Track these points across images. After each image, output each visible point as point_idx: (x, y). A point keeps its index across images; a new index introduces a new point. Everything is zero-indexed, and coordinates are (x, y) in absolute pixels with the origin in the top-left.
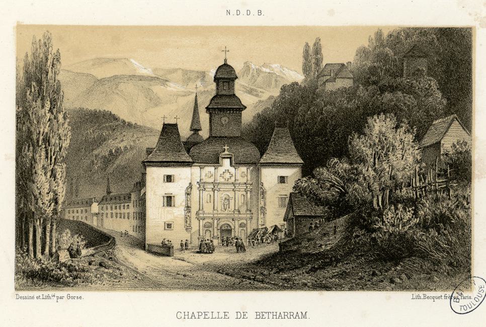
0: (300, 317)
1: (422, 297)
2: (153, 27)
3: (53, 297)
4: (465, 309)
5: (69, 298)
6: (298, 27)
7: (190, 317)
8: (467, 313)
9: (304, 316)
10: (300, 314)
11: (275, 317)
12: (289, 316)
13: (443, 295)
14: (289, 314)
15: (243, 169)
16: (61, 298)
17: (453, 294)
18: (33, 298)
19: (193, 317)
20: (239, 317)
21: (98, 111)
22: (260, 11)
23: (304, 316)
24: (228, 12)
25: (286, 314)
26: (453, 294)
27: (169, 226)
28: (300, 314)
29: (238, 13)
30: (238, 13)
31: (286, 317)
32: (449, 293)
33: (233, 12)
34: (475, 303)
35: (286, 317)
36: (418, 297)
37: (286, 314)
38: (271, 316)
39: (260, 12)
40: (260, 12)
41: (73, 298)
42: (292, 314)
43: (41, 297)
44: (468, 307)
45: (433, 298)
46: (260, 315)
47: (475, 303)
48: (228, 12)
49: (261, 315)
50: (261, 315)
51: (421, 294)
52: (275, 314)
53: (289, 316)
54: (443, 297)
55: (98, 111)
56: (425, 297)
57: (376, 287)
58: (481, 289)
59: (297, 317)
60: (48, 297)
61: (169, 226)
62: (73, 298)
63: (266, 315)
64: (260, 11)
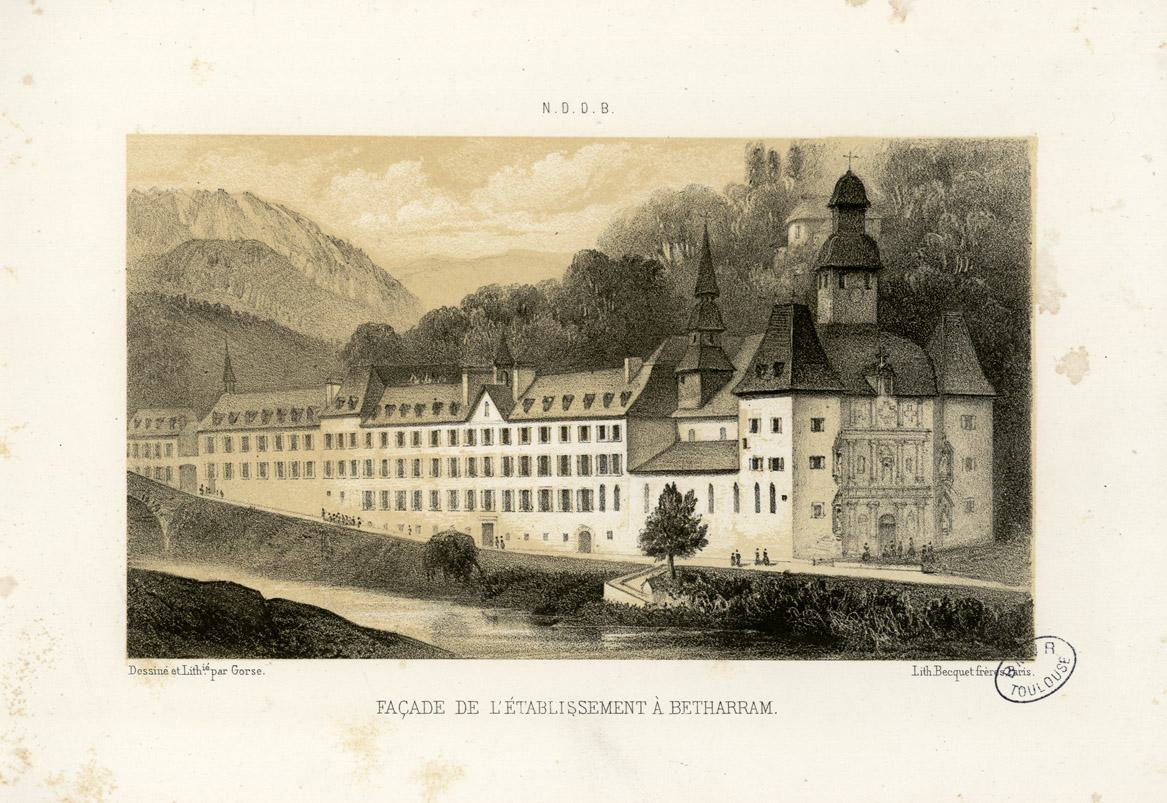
1: (933, 671)
3: (206, 671)
4: (1032, 692)
7: (715, 711)
8: (1024, 702)
9: (766, 708)
11: (709, 711)
12: (737, 707)
13: (974, 668)
14: (737, 704)
15: (550, 156)
18: (165, 672)
19: (391, 711)
20: (462, 711)
22: (605, 106)
24: (546, 107)
25: (732, 704)
27: (28, 80)
28: (759, 706)
31: (731, 710)
32: (993, 665)
33: (575, 106)
35: (731, 710)
36: (925, 672)
37: (732, 704)
39: (605, 108)
40: (605, 108)
41: (243, 672)
42: (743, 705)
44: (1028, 692)
45: (956, 673)
46: (679, 707)
48: (546, 107)
49: (681, 706)
50: (681, 706)
51: (931, 664)
52: (709, 711)
53: (737, 707)
54: (974, 673)
57: (817, 656)
58: (1063, 664)
59: (531, 711)
60: (196, 671)
61: (28, 80)
63: (515, 707)
64: (605, 106)
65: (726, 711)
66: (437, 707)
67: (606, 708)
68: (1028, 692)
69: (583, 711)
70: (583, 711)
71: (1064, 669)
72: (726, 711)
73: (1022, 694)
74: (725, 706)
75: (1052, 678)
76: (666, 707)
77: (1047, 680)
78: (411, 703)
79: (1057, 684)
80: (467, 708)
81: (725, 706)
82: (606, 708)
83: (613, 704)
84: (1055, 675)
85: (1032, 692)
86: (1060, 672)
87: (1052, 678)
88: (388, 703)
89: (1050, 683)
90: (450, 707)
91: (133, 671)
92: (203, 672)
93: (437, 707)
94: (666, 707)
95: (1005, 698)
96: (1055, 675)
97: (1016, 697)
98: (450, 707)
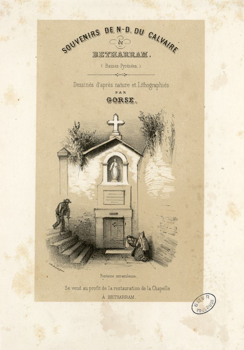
9: (145, 55)
14: (125, 296)
20: (75, 86)
28: (131, 297)
31: (123, 298)
34: (206, 309)
35: (123, 298)
47: (206, 309)
59: (129, 298)
65: (122, 298)
67: (120, 100)
69: (83, 86)
70: (83, 86)
71: (212, 303)
72: (122, 298)
73: (200, 311)
74: (122, 296)
79: (210, 308)
81: (122, 296)
82: (120, 100)
86: (211, 304)
88: (154, 35)
90: (102, 31)
95: (194, 312)
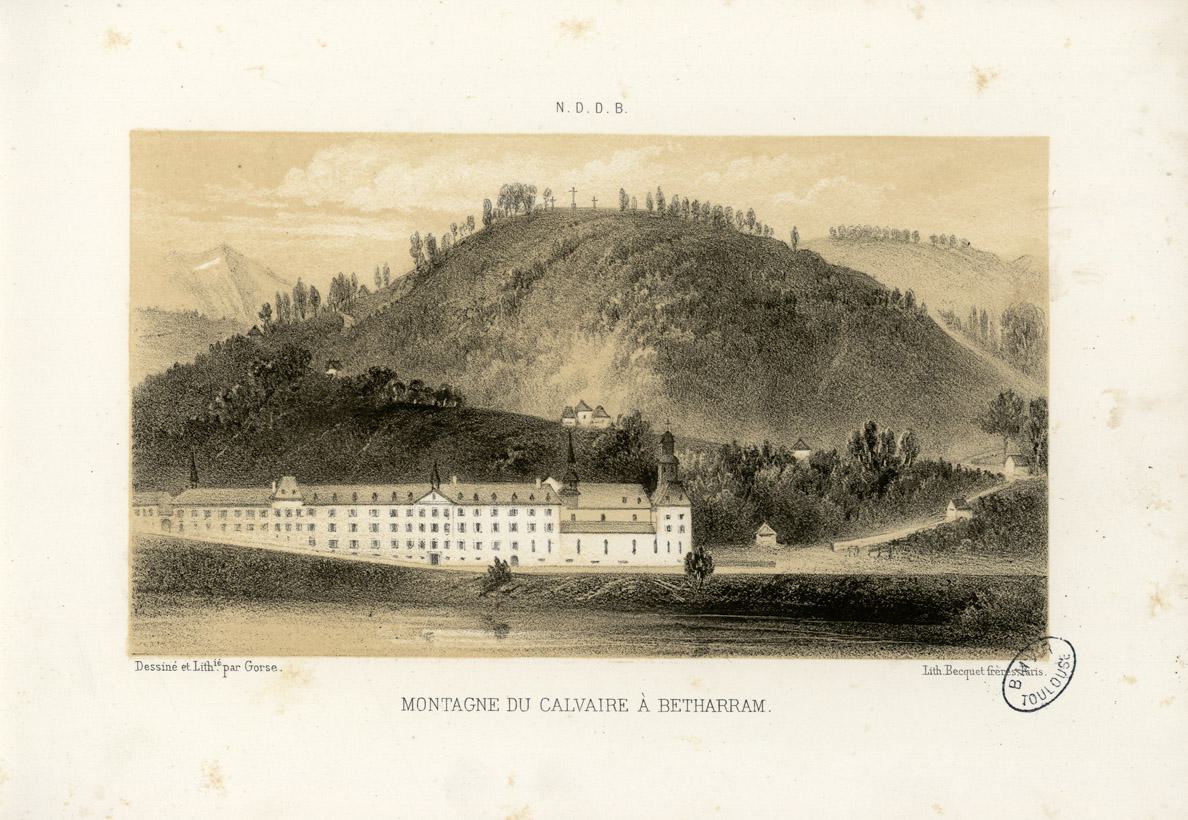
0: (564, 708)
1: (944, 671)
2: (818, 139)
4: (1043, 697)
5: (249, 668)
6: (996, 141)
9: (760, 706)
10: (751, 704)
13: (985, 668)
14: (729, 702)
16: (233, 668)
17: (1010, 665)
19: (710, 710)
21: (325, 293)
22: (619, 110)
23: (409, 704)
24: (560, 106)
26: (1010, 665)
28: (751, 704)
29: (579, 107)
30: (579, 107)
33: (590, 106)
34: (1016, 678)
35: (734, 708)
36: (937, 671)
38: (692, 706)
39: (619, 107)
40: (619, 107)
41: (258, 668)
43: (192, 667)
44: (1038, 698)
46: (669, 705)
48: (560, 106)
49: (670, 705)
50: (670, 705)
53: (728, 706)
54: (986, 672)
55: (325, 293)
56: (950, 671)
62: (258, 668)
66: (620, 705)
68: (1038, 698)
75: (1037, 695)
76: (653, 705)
77: (1054, 681)
78: (553, 701)
80: (517, 704)
83: (488, 701)
84: (1041, 693)
85: (1043, 697)
87: (1037, 695)
88: (454, 700)
89: (1033, 700)
90: (503, 704)
91: (142, 667)
92: (214, 668)
93: (620, 705)
94: (653, 705)
96: (1041, 693)
97: (1029, 706)
98: (503, 704)
